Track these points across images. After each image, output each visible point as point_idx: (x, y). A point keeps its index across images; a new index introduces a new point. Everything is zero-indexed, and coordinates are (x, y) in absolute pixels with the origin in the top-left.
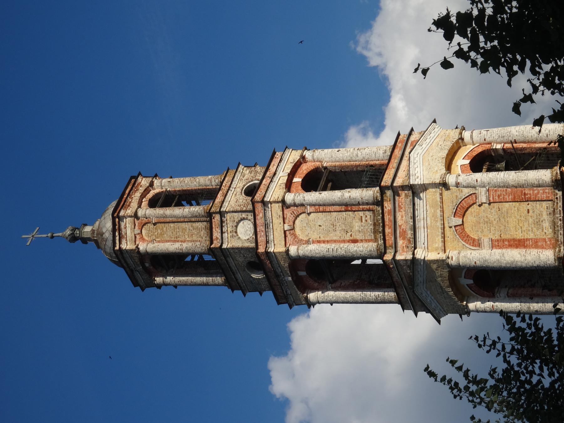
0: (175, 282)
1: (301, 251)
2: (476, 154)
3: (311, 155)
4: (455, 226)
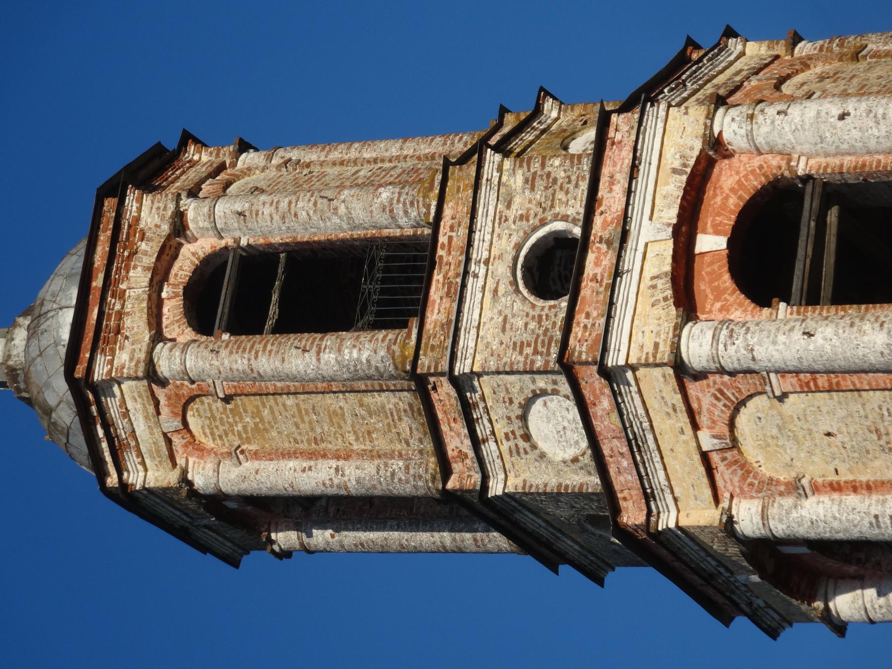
0: (342, 546)
3: (743, 132)
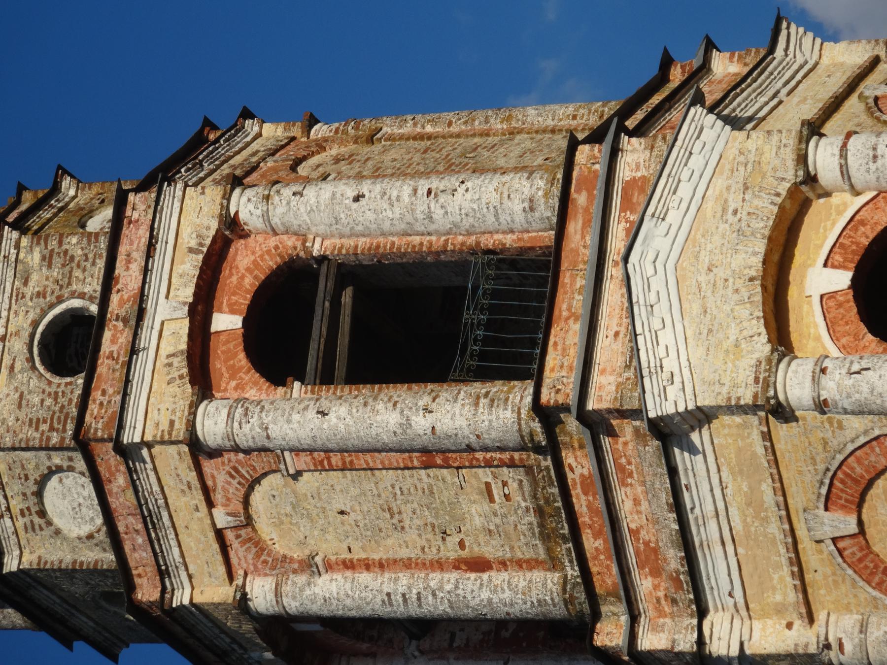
1: (290, 600)
2: (872, 236)
3: (259, 212)
4: (834, 540)
